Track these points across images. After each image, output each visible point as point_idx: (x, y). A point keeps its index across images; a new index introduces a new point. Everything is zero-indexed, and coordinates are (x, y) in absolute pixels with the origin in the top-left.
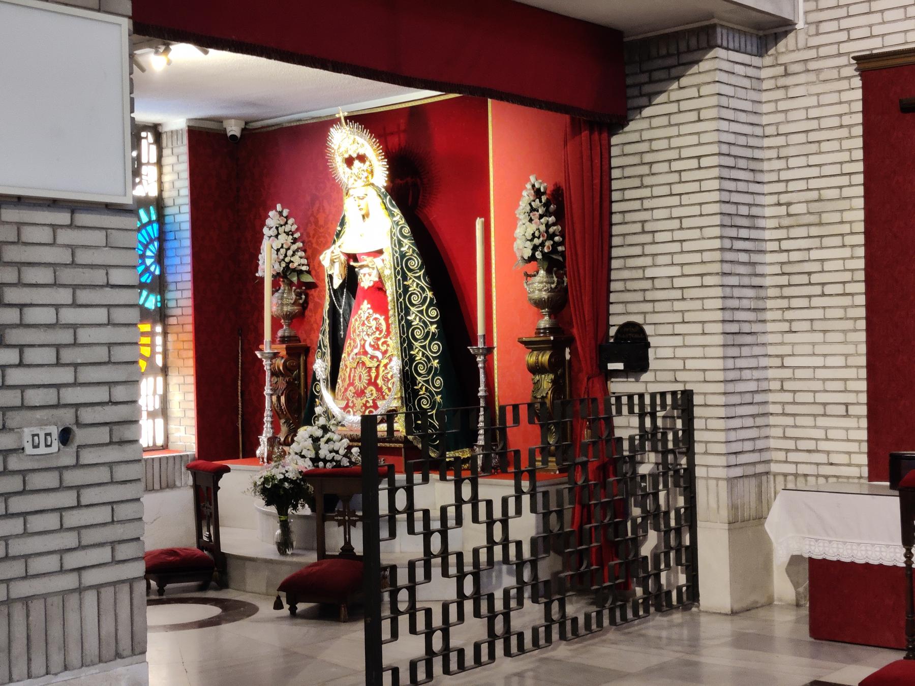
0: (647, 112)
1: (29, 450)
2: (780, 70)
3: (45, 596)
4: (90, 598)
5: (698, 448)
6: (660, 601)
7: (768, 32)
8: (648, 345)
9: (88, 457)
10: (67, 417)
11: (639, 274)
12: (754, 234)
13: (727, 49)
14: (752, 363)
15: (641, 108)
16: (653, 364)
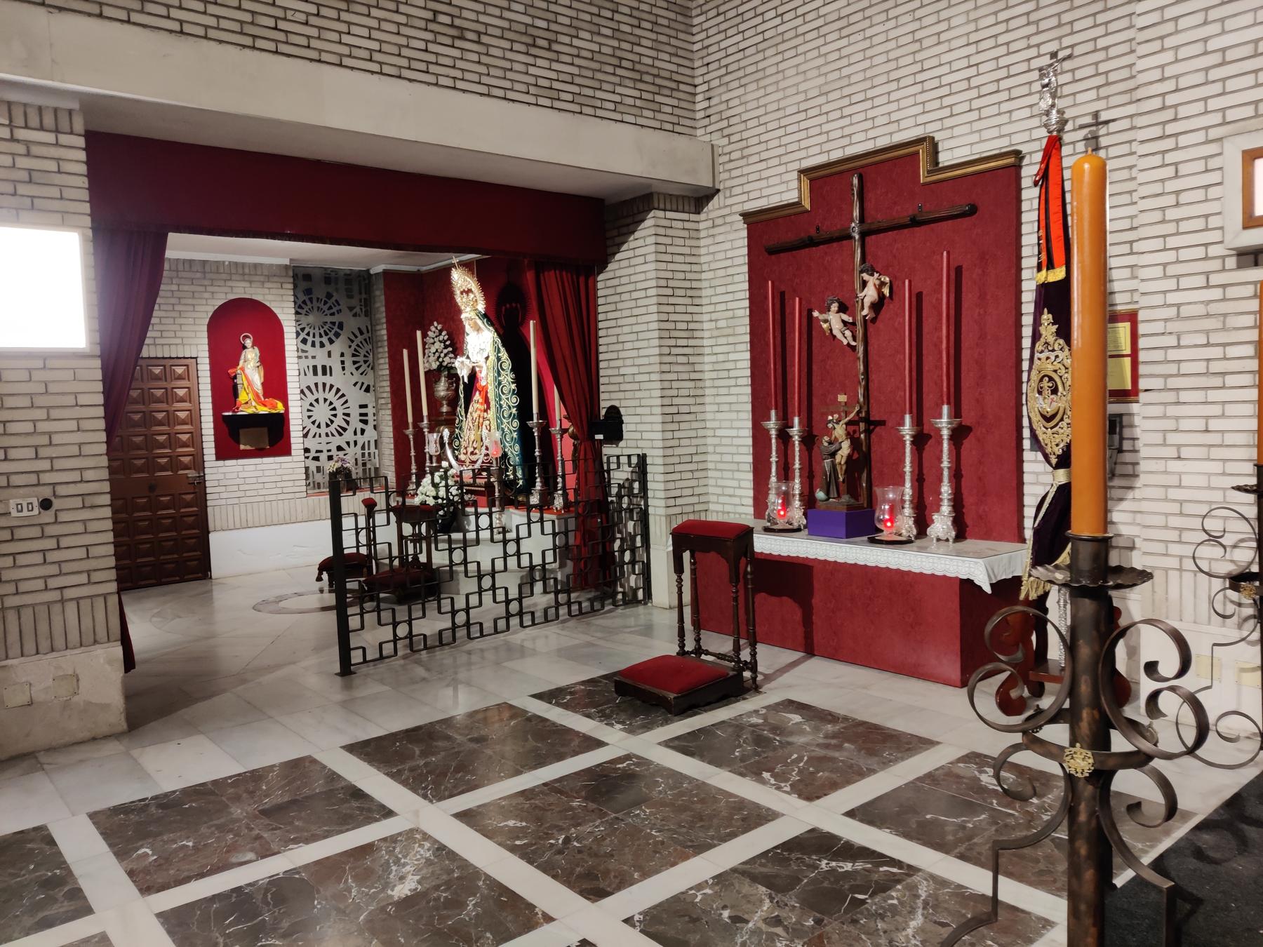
0: (618, 257)
1: (14, 513)
2: (1170, 171)
3: (33, 606)
4: (71, 608)
5: (650, 494)
6: (631, 600)
7: (698, 199)
8: (622, 422)
9: (63, 517)
10: (46, 492)
11: (615, 372)
12: (691, 342)
13: (665, 210)
14: (693, 434)
15: (615, 254)
16: (625, 435)
